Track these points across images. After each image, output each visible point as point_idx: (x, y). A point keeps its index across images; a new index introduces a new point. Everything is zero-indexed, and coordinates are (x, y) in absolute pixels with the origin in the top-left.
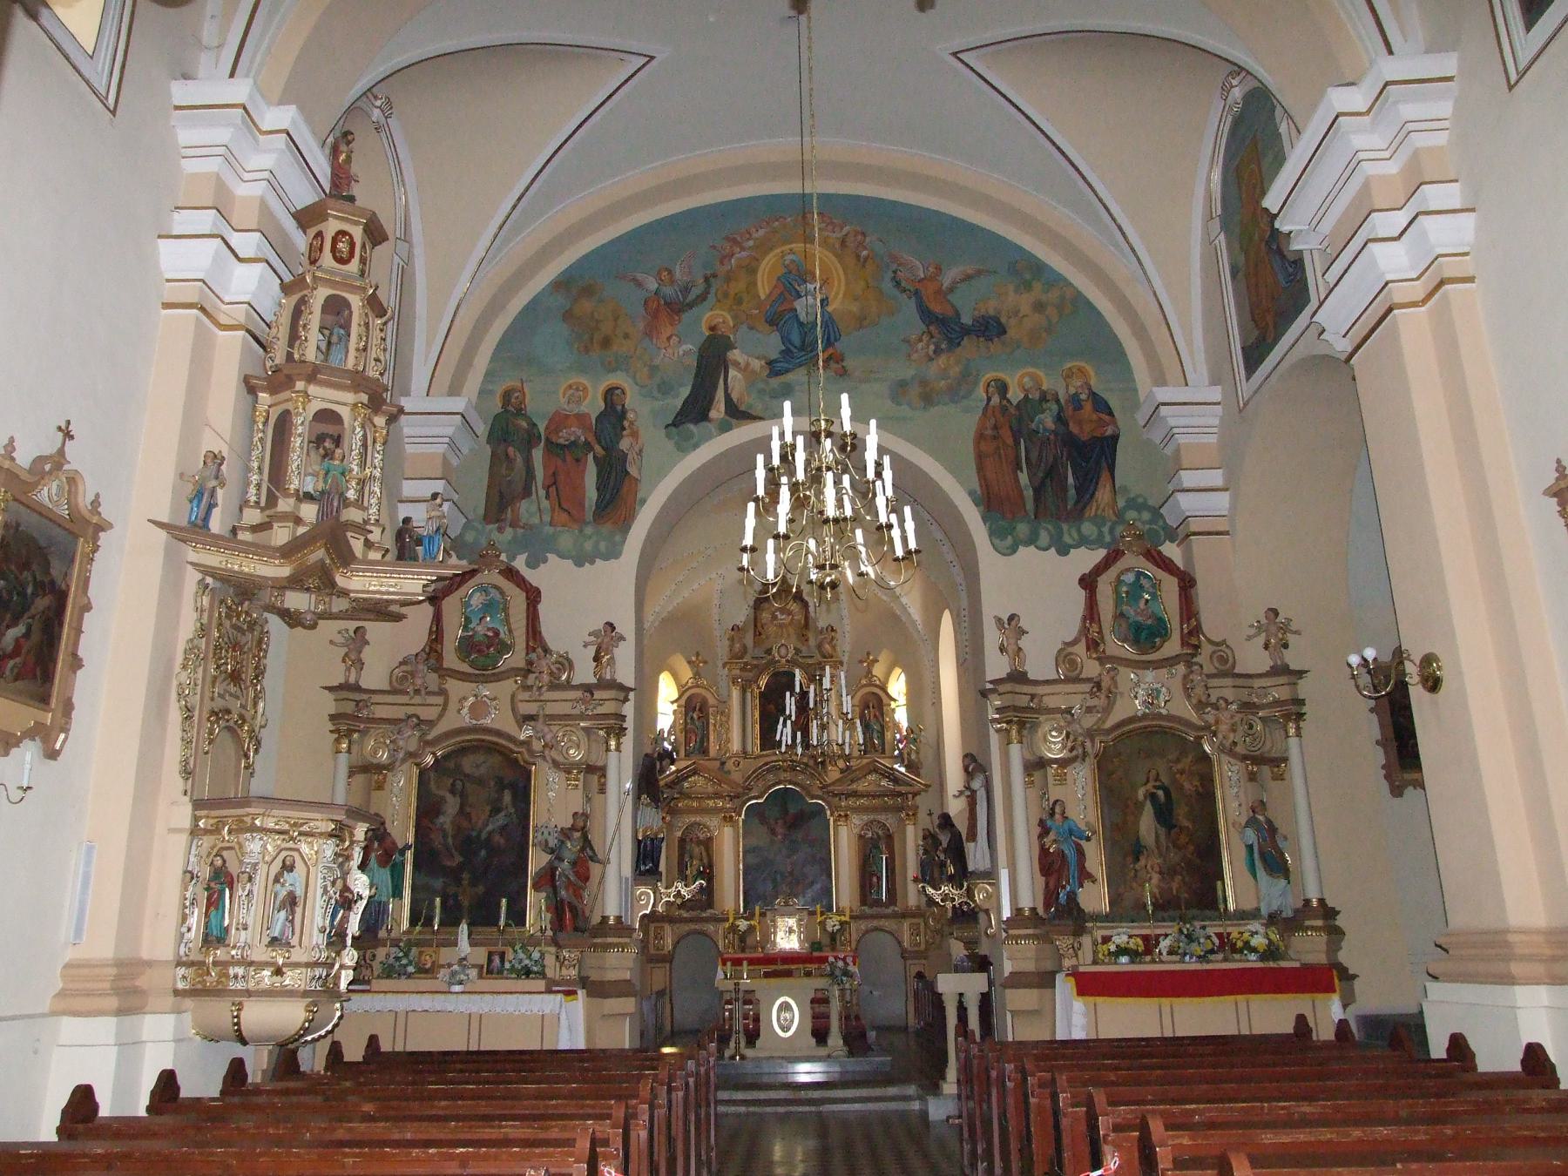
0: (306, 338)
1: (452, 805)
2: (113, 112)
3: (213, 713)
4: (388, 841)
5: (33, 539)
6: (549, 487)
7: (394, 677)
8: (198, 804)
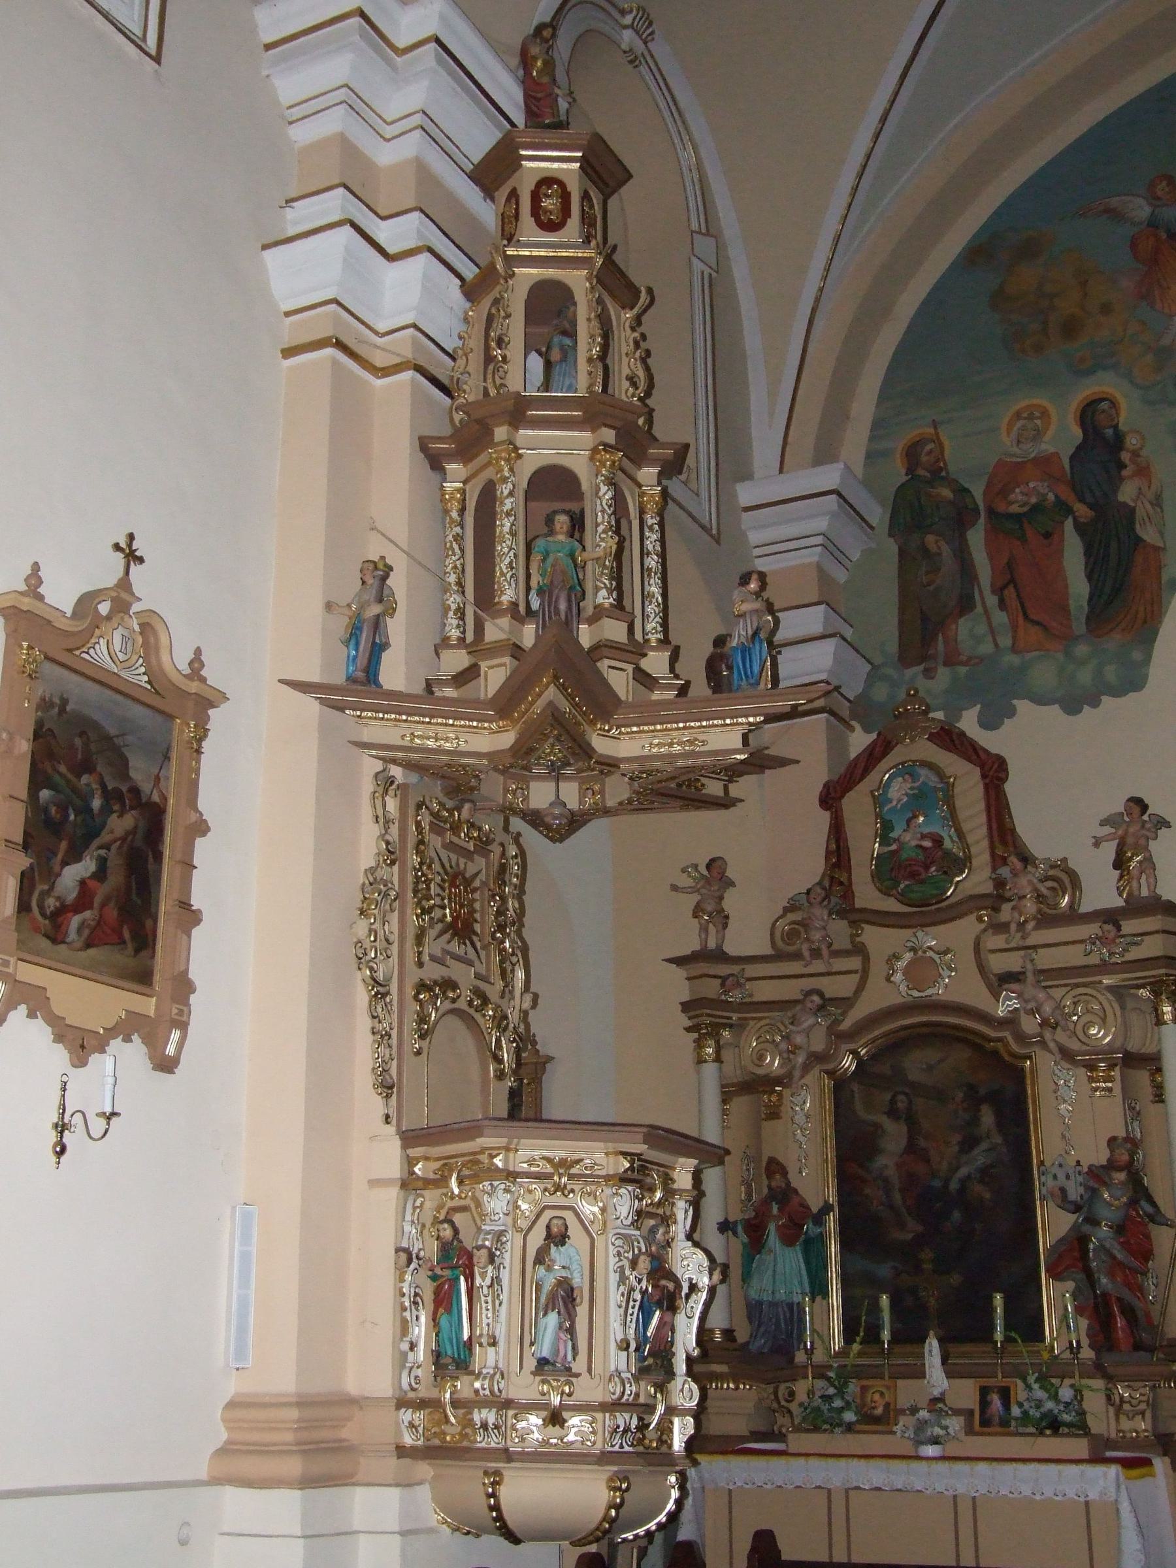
0: (504, 358)
1: (894, 1137)
2: (157, 59)
3: (422, 986)
4: (795, 1201)
5: (95, 725)
6: (1002, 589)
7: (778, 934)
8: (409, 1138)
